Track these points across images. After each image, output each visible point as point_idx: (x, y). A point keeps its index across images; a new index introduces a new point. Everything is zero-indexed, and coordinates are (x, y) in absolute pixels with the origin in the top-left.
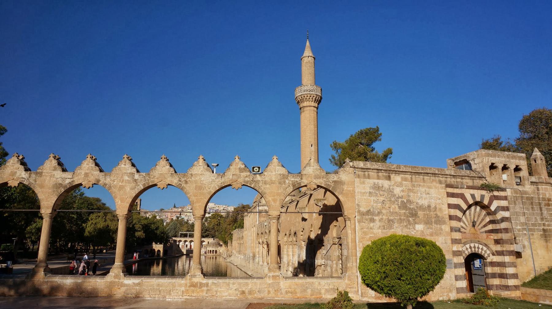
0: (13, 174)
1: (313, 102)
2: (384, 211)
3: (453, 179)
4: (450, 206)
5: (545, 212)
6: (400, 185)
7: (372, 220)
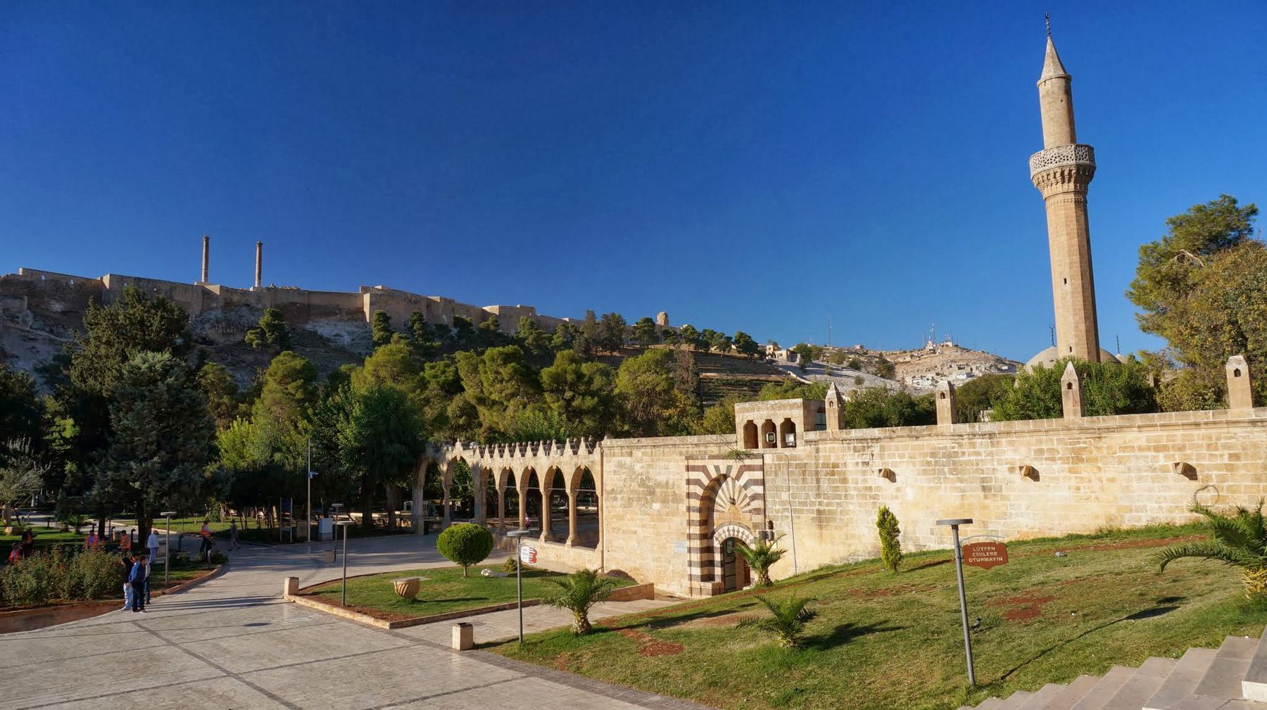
1: (1060, 184)
2: (625, 489)
3: (696, 449)
4: (689, 482)
5: (824, 485)
6: (640, 461)
7: (615, 499)
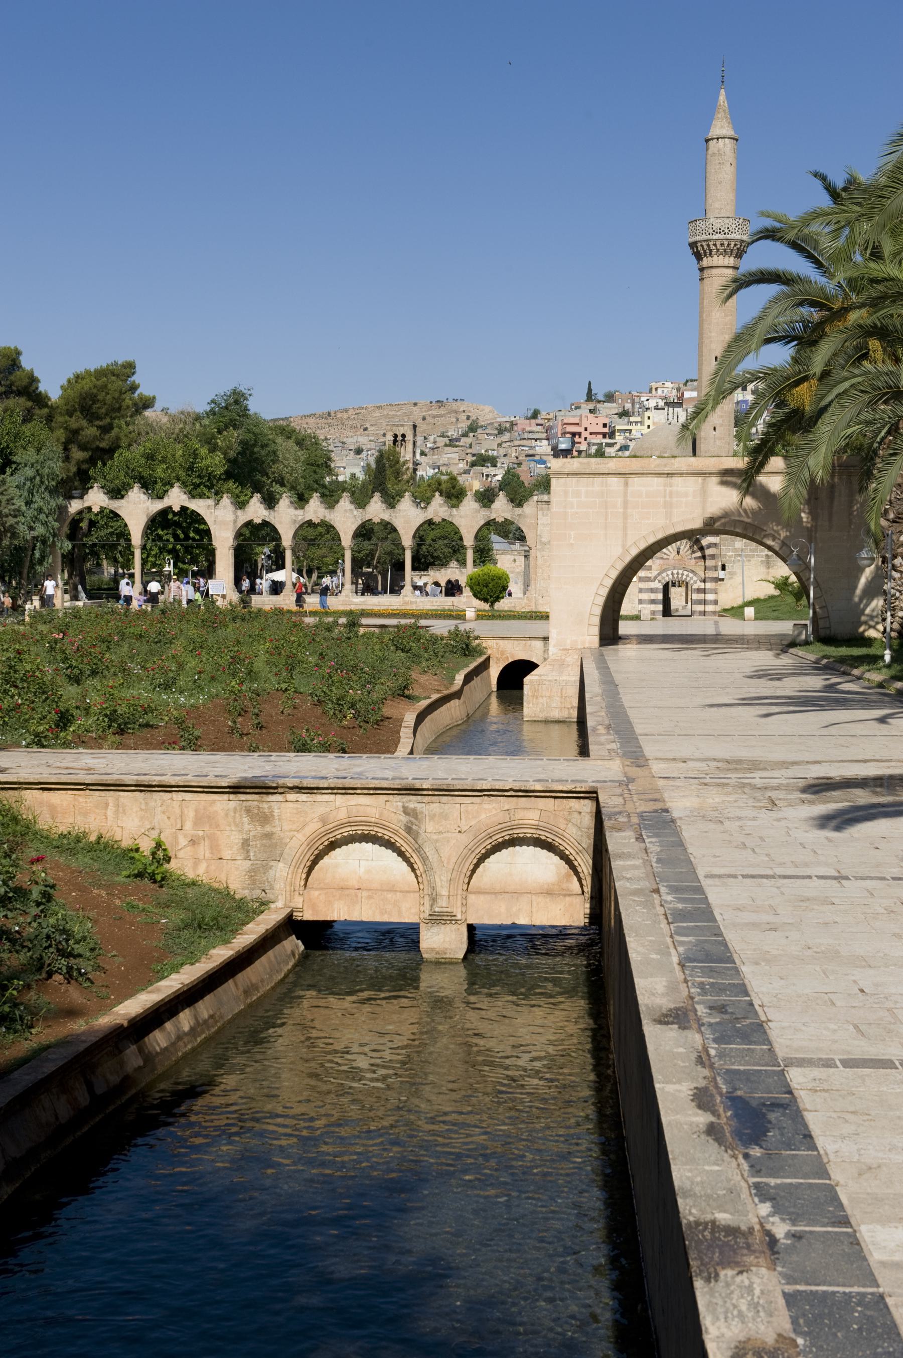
0: (256, 512)
